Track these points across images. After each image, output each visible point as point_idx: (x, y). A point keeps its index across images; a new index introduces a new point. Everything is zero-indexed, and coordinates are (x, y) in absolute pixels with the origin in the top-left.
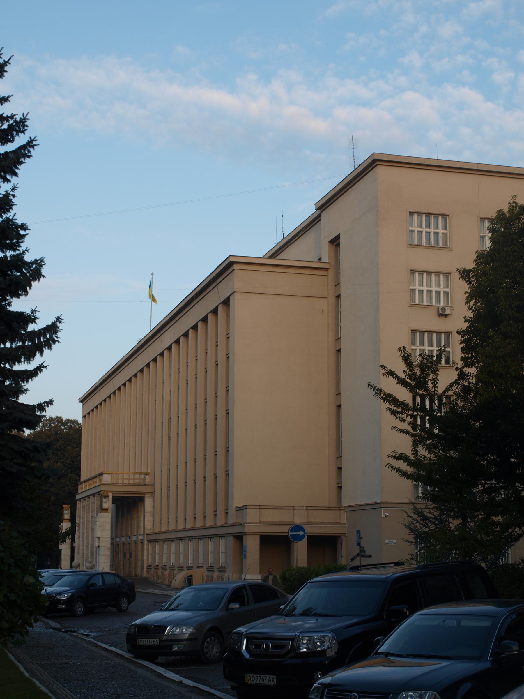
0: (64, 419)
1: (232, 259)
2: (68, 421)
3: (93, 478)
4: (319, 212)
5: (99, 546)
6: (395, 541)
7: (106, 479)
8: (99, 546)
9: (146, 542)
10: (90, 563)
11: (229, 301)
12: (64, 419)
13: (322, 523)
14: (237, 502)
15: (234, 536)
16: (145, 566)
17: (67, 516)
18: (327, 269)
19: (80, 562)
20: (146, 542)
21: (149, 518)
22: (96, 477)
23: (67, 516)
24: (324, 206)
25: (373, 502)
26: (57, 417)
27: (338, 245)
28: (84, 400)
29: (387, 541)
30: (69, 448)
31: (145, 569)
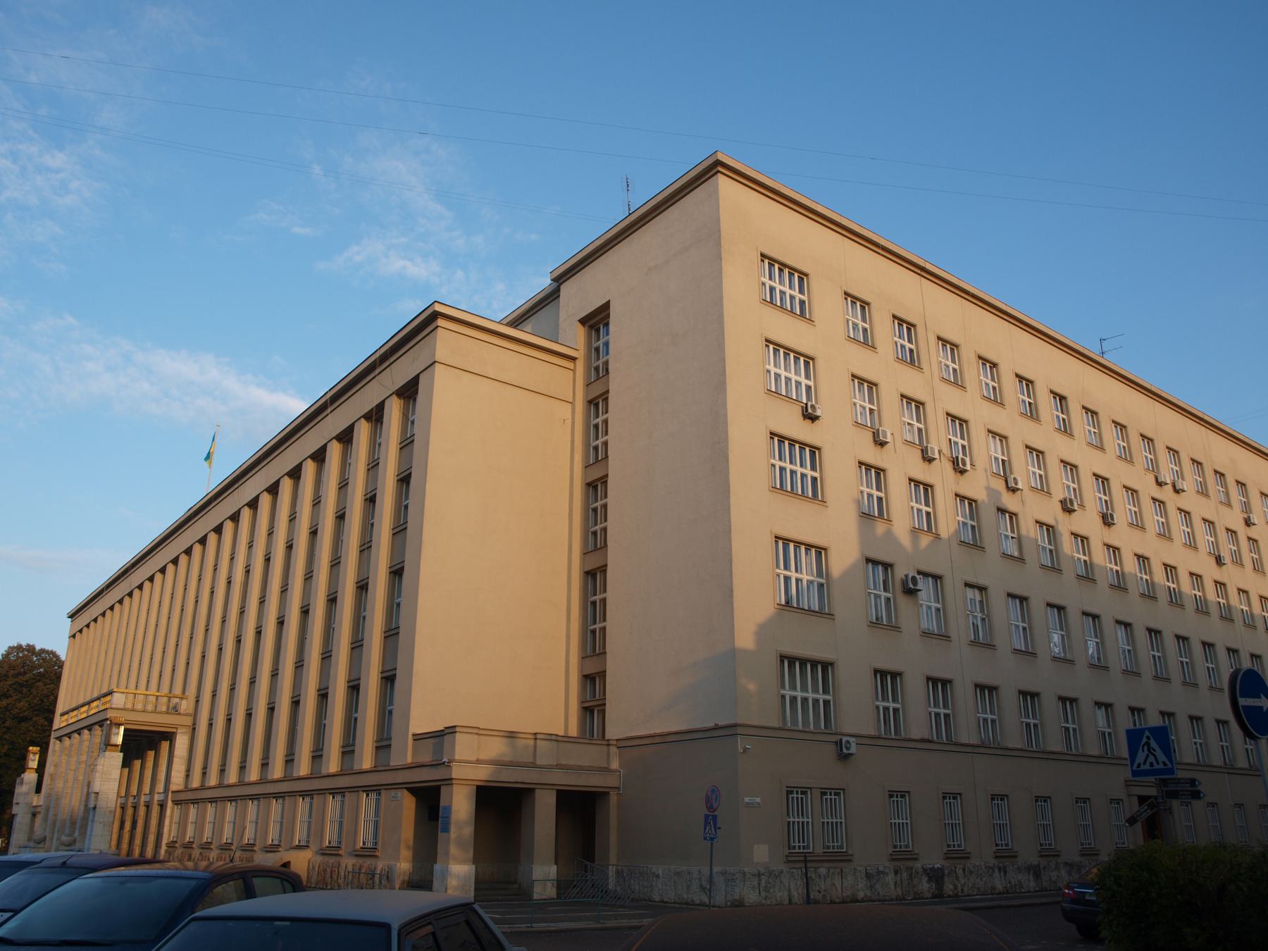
0: (38, 648)
1: (438, 308)
2: (43, 651)
3: (89, 703)
4: (555, 284)
5: (95, 808)
6: (758, 800)
7: (118, 700)
8: (95, 808)
9: (170, 804)
10: (70, 835)
11: (417, 383)
12: (38, 648)
13: (581, 768)
14: (423, 715)
15: (409, 789)
16: (165, 841)
17: (33, 762)
18: (573, 359)
19: (48, 834)
20: (170, 804)
21: (176, 767)
22: (83, 706)
23: (33, 762)
24: (561, 278)
25: (711, 724)
26: (28, 645)
27: (408, 483)
28: (72, 616)
29: (747, 800)
30: (40, 684)
31: (164, 848)
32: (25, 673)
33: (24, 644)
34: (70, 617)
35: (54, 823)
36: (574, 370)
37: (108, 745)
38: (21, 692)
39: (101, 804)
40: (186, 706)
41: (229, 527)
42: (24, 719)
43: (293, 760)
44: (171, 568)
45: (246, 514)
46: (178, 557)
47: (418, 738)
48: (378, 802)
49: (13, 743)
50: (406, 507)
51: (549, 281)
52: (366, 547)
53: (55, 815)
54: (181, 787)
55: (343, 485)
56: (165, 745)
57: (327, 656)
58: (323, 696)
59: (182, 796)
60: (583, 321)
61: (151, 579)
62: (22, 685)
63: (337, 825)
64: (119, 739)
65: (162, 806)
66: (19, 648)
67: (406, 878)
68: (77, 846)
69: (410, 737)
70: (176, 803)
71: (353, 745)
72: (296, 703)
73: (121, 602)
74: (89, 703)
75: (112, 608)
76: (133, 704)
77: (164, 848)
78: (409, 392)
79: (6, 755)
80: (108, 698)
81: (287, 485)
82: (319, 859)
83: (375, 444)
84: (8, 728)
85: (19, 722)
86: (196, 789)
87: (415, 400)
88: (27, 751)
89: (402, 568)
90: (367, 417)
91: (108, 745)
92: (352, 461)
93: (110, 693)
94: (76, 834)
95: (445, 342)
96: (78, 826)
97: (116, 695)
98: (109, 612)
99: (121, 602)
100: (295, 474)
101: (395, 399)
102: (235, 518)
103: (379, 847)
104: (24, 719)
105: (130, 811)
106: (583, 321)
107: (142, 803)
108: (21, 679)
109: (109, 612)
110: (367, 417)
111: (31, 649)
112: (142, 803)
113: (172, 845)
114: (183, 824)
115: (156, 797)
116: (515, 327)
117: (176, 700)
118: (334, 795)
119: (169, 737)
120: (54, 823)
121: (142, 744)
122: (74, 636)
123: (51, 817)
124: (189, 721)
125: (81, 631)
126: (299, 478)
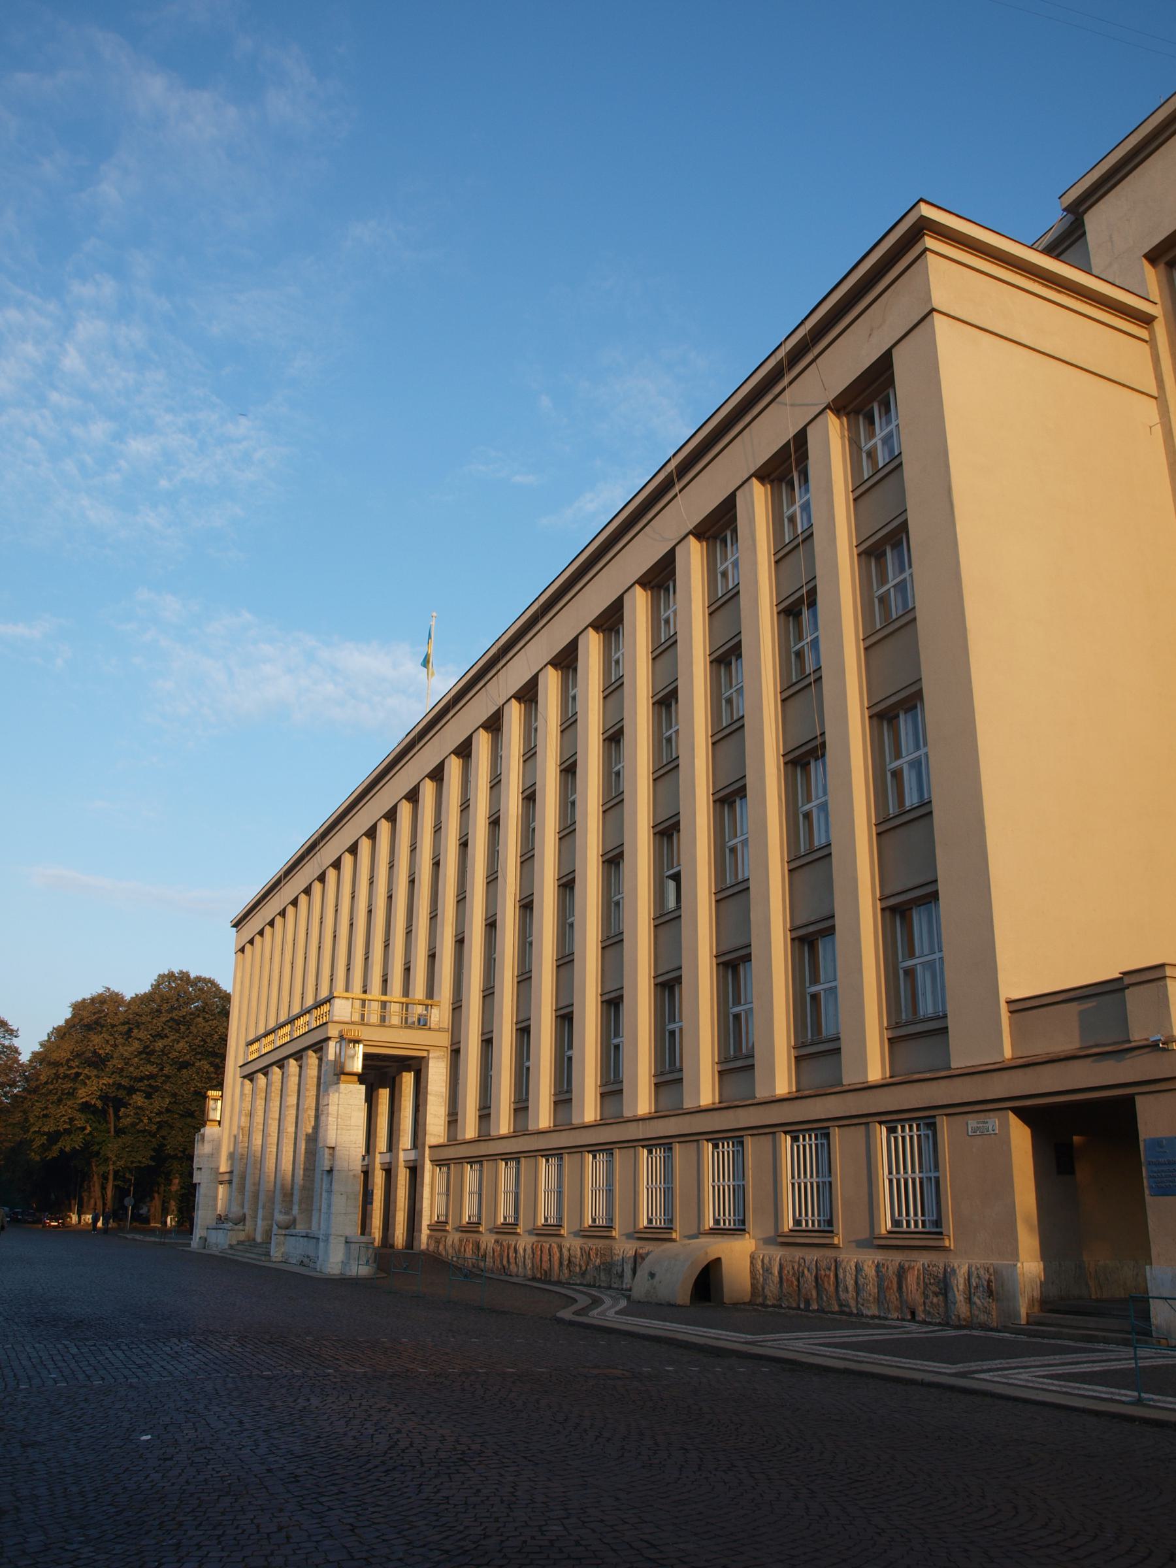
0: (193, 975)
2: (199, 979)
3: (291, 1021)
4: (1071, 218)
5: (330, 1171)
7: (343, 1010)
8: (330, 1171)
9: (428, 1165)
10: (287, 1213)
12: (193, 975)
16: (425, 1222)
19: (247, 1211)
20: (428, 1165)
26: (181, 972)
28: (237, 924)
30: (200, 1019)
31: (425, 1232)
32: (179, 1008)
33: (176, 971)
34: (236, 925)
35: (256, 1195)
36: (1152, 343)
37: (340, 1072)
38: (178, 1031)
39: (339, 1165)
40: (440, 1016)
41: (365, 845)
42: (185, 1065)
43: (489, 1115)
44: (303, 899)
45: (384, 828)
46: (284, 909)
47: (1020, 1007)
48: (560, 1167)
49: (175, 1095)
50: (573, 803)
51: (1058, 214)
52: (528, 858)
53: (258, 1184)
54: (442, 1140)
55: (530, 755)
56: (408, 1079)
57: (489, 993)
58: (565, 1019)
59: (451, 1153)
60: (1152, 257)
61: (294, 903)
62: (178, 1023)
63: (512, 1196)
64: (357, 1066)
65: (414, 1171)
66: (171, 975)
67: (1037, 1294)
68: (300, 1228)
69: (1004, 1008)
70: (438, 1163)
71: (527, 1100)
72: (487, 1042)
73: (261, 933)
74: (291, 1021)
75: (271, 924)
76: (360, 1020)
77: (425, 1232)
78: (869, 397)
79: (168, 1110)
80: (326, 1008)
81: (405, 809)
82: (777, 1254)
83: (569, 700)
84: (168, 1077)
85: (179, 1070)
86: (643, 1119)
87: (575, 670)
88: (205, 1097)
89: (573, 880)
90: (555, 663)
91: (340, 1072)
92: (540, 724)
93: (329, 1000)
94: (295, 1210)
95: (946, 277)
96: (296, 1198)
97: (337, 1003)
98: (258, 939)
99: (261, 933)
100: (437, 775)
101: (756, 485)
102: (371, 833)
103: (949, 1226)
104: (185, 1065)
105: (379, 1178)
106: (1152, 257)
107: (402, 1164)
108: (175, 1014)
109: (268, 929)
110: (555, 663)
111: (184, 977)
112: (378, 1166)
113: (438, 1227)
114: (453, 1193)
115: (378, 1159)
116: (1057, 257)
117: (420, 1010)
118: (506, 1160)
119: (416, 1065)
120: (256, 1195)
121: (382, 1073)
122: (242, 950)
123: (249, 1186)
124: (445, 1039)
125: (251, 942)
126: (442, 779)
